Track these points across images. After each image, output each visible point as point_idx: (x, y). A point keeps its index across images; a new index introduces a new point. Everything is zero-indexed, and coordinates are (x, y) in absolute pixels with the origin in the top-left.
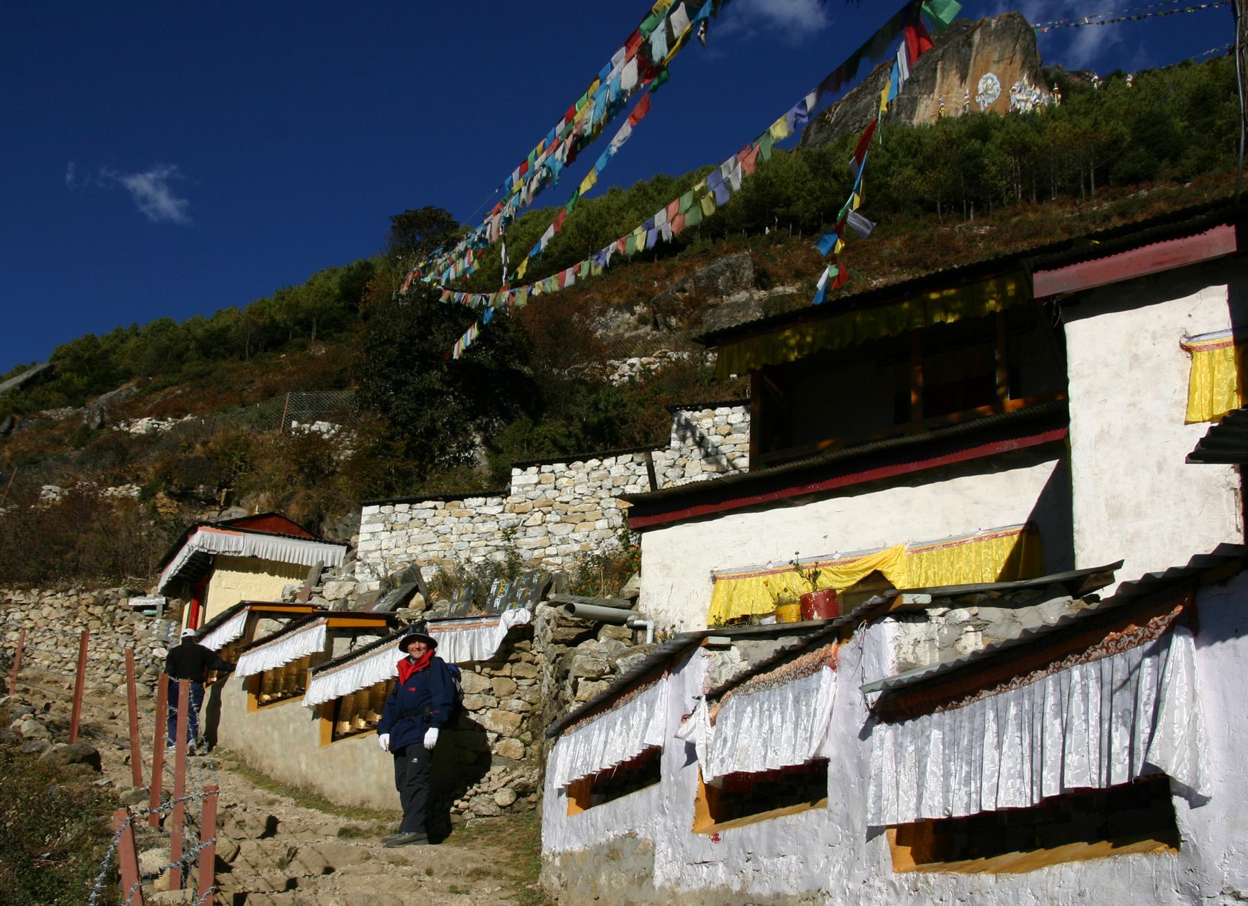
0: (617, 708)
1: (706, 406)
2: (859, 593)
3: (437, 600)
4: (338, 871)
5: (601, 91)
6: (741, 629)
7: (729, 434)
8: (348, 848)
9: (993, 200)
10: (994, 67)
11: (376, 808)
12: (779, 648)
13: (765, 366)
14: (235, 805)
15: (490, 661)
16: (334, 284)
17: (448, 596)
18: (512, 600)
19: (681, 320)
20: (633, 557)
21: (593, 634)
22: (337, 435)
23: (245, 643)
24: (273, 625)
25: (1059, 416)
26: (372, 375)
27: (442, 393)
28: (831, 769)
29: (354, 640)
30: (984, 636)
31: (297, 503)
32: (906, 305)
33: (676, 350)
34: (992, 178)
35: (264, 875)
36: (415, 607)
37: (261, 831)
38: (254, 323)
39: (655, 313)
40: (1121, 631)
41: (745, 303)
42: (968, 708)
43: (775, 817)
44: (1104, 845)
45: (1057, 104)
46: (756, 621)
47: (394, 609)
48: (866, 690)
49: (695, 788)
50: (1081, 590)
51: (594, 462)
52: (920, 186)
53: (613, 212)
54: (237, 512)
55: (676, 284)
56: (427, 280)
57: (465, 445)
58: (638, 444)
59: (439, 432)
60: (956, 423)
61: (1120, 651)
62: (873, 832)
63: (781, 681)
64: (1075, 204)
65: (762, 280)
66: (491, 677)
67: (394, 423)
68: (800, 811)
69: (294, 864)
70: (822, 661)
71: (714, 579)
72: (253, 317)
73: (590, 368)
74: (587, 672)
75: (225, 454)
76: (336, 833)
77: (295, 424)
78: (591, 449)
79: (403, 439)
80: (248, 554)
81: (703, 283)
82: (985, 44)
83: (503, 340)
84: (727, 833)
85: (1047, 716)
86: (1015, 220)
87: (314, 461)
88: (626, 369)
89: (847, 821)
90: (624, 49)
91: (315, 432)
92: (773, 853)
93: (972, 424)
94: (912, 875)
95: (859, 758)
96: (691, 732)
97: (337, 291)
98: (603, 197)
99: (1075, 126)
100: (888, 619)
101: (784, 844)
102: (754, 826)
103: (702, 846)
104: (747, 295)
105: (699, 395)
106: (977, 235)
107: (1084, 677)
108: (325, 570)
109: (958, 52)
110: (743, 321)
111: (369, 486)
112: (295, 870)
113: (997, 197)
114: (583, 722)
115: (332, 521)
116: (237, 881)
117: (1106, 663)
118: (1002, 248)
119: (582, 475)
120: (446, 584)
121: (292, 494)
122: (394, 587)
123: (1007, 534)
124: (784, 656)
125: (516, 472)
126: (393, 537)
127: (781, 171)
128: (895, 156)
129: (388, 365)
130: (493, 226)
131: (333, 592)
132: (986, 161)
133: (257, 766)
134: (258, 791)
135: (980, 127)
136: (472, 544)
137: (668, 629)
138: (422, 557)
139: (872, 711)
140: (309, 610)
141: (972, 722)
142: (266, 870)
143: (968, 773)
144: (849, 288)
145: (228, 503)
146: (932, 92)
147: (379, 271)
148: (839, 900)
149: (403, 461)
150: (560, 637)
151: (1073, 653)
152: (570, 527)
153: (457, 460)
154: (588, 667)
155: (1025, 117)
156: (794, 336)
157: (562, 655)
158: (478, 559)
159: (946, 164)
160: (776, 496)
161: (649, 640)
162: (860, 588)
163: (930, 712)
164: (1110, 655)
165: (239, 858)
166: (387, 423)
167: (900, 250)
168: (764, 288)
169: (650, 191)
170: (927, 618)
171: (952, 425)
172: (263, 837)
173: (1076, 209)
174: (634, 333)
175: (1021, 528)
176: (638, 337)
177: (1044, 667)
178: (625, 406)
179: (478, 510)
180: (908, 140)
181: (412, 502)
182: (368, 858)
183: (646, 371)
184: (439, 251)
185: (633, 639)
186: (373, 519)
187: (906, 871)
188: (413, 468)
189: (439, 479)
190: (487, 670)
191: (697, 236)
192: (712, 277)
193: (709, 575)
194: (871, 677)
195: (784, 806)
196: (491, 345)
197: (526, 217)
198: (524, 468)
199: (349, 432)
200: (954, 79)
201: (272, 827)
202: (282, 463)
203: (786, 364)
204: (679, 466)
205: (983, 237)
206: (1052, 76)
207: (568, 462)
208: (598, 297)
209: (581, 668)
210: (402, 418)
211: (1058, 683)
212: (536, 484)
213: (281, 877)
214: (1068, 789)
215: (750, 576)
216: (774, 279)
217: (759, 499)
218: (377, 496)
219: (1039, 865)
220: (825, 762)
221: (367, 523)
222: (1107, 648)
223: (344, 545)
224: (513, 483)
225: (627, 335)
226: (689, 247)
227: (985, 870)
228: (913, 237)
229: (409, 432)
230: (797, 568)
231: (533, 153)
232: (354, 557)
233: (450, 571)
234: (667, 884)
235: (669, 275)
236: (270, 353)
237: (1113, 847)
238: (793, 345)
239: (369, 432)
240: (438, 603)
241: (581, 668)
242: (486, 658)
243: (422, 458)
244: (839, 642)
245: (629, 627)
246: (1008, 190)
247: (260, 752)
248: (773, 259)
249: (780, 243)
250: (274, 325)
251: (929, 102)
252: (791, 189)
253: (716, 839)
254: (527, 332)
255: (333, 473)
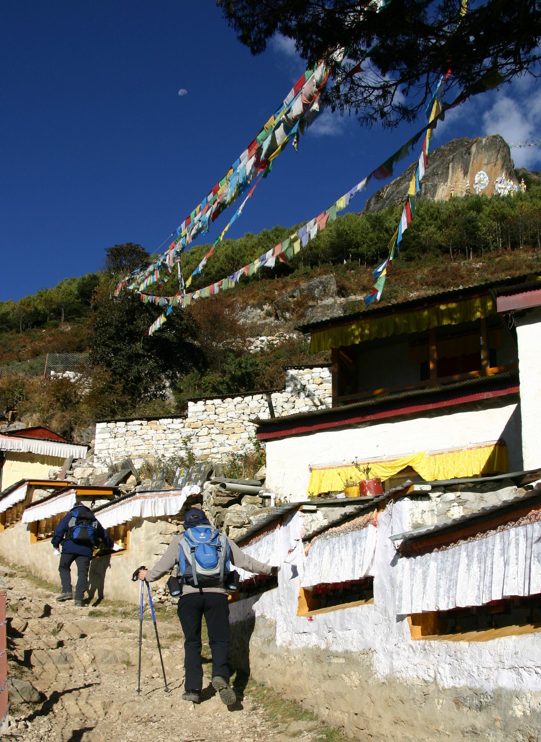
0: (251, 544)
1: (307, 367)
2: (399, 478)
3: (144, 479)
4: (89, 636)
5: (234, 176)
6: (325, 500)
7: (321, 383)
8: (96, 623)
9: (484, 248)
10: (485, 168)
11: (112, 599)
12: (343, 513)
13: (341, 346)
14: (25, 598)
15: (177, 515)
16: (74, 288)
17: (151, 477)
18: (188, 480)
19: (292, 314)
20: (262, 456)
21: (238, 501)
22: (80, 380)
23: (27, 503)
24: (45, 493)
25: (514, 381)
26: (99, 344)
27: (144, 356)
28: (375, 582)
29: (94, 502)
30: (464, 508)
31: (56, 420)
32: (426, 313)
33: (288, 332)
34: (483, 234)
35: (43, 639)
36: (130, 483)
37: (41, 614)
38: (24, 311)
39: (276, 310)
40: (538, 509)
41: (331, 306)
42: (452, 550)
43: (344, 608)
44: (529, 627)
45: (523, 191)
46: (333, 495)
47: (117, 484)
48: (394, 539)
49: (298, 591)
50: (522, 483)
51: (239, 399)
52: (439, 237)
53: (248, 248)
54: (18, 426)
55: (289, 291)
56: (131, 287)
57: (160, 387)
58: (266, 388)
59: (143, 379)
60: (457, 381)
61: (538, 520)
62: (400, 618)
63: (345, 532)
64: (534, 251)
65: (342, 291)
66: (178, 524)
67: (114, 373)
68: (358, 605)
69: (62, 632)
70: (368, 521)
71: (311, 470)
72: (23, 307)
73: (236, 343)
74: (234, 523)
75: (10, 391)
76: (87, 614)
77: (52, 373)
78: (238, 391)
79: (121, 383)
80: (26, 451)
81: (305, 293)
82: (479, 153)
83: (181, 325)
84: (317, 616)
85: (495, 556)
86: (497, 260)
87: (65, 395)
88: (258, 343)
89: (385, 611)
90: (247, 151)
91: (66, 378)
92: (343, 628)
93: (465, 383)
94: (422, 642)
95: (391, 576)
96: (293, 560)
97: (76, 292)
98: (243, 239)
99: (534, 205)
100: (406, 499)
101: (347, 623)
102: (332, 613)
103: (303, 623)
104: (333, 300)
105: (303, 360)
106: (474, 269)
107: (517, 535)
108: (74, 461)
109: (463, 157)
110: (331, 315)
111: (101, 411)
112: (62, 636)
113: (487, 245)
114: (253, 541)
115: (79, 431)
116: (27, 643)
117: (529, 526)
118: (489, 276)
119: (231, 406)
120: (149, 470)
121: (53, 415)
122: (117, 471)
123: (487, 446)
124: (347, 518)
125: (190, 404)
126: (116, 442)
127: (353, 227)
128: (423, 219)
129: (109, 338)
130: (169, 257)
131: (79, 474)
132: (480, 224)
133: (38, 575)
134: (40, 590)
135: (476, 204)
136: (165, 446)
137: (282, 499)
138: (135, 453)
139: (397, 550)
140: (66, 484)
141: (453, 558)
142: (44, 636)
143: (450, 586)
144: (396, 298)
145: (13, 419)
146: (446, 181)
147: (102, 280)
148: (382, 655)
149: (121, 396)
150: (218, 503)
151: (511, 521)
152: (225, 437)
153: (155, 396)
154: (235, 520)
155: (503, 198)
156: (357, 328)
157: (220, 512)
158: (169, 455)
159: (455, 225)
160: (347, 422)
161: (273, 505)
162: (400, 476)
163: (430, 551)
164: (532, 523)
165: (28, 630)
166: (111, 373)
167: (427, 276)
168: (343, 296)
169: (271, 236)
170: (429, 498)
171: (455, 382)
172: (42, 617)
173: (535, 254)
174: (263, 322)
175: (495, 443)
176: (266, 324)
177: (495, 528)
178: (257, 365)
179: (169, 426)
180: (431, 210)
181: (127, 421)
182: (107, 629)
183: (270, 345)
184: (138, 270)
185: (263, 503)
186: (103, 431)
187: (419, 639)
188: (126, 401)
189: (144, 407)
190: (175, 521)
191: (301, 265)
192: (311, 290)
193: (308, 467)
194: (397, 531)
195: (349, 602)
196: (174, 328)
197: (194, 250)
198: (195, 401)
199: (87, 378)
200: (460, 174)
201: (47, 611)
202: (46, 396)
203: (354, 345)
204: (286, 404)
205: (478, 269)
206: (520, 174)
207: (223, 398)
208: (240, 300)
209: (230, 520)
210: (119, 370)
211: (502, 538)
212: (203, 411)
213: (54, 640)
214: (505, 596)
215: (332, 468)
216: (349, 291)
217: (337, 424)
218: (106, 417)
219: (493, 638)
220: (372, 578)
221: (99, 433)
222: (530, 519)
223: (86, 446)
224: (189, 410)
225: (259, 323)
226: (296, 270)
227: (463, 640)
228: (435, 268)
229: (124, 379)
230: (357, 465)
231: (193, 213)
232: (93, 453)
233: (152, 462)
234: (284, 644)
235: (284, 287)
236: (35, 329)
237: (534, 628)
238: (357, 333)
239: (99, 378)
240: (144, 481)
241: (230, 520)
242: (174, 514)
243: (133, 394)
244: (378, 511)
245: (260, 497)
246: (493, 242)
247: (40, 567)
248: (348, 279)
249: (353, 269)
250: (37, 312)
251: (445, 187)
252: (359, 237)
253: (311, 620)
254: (195, 320)
255: (78, 402)
